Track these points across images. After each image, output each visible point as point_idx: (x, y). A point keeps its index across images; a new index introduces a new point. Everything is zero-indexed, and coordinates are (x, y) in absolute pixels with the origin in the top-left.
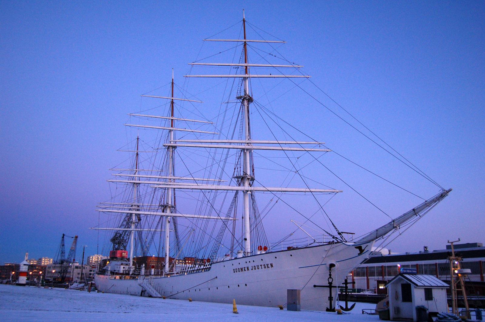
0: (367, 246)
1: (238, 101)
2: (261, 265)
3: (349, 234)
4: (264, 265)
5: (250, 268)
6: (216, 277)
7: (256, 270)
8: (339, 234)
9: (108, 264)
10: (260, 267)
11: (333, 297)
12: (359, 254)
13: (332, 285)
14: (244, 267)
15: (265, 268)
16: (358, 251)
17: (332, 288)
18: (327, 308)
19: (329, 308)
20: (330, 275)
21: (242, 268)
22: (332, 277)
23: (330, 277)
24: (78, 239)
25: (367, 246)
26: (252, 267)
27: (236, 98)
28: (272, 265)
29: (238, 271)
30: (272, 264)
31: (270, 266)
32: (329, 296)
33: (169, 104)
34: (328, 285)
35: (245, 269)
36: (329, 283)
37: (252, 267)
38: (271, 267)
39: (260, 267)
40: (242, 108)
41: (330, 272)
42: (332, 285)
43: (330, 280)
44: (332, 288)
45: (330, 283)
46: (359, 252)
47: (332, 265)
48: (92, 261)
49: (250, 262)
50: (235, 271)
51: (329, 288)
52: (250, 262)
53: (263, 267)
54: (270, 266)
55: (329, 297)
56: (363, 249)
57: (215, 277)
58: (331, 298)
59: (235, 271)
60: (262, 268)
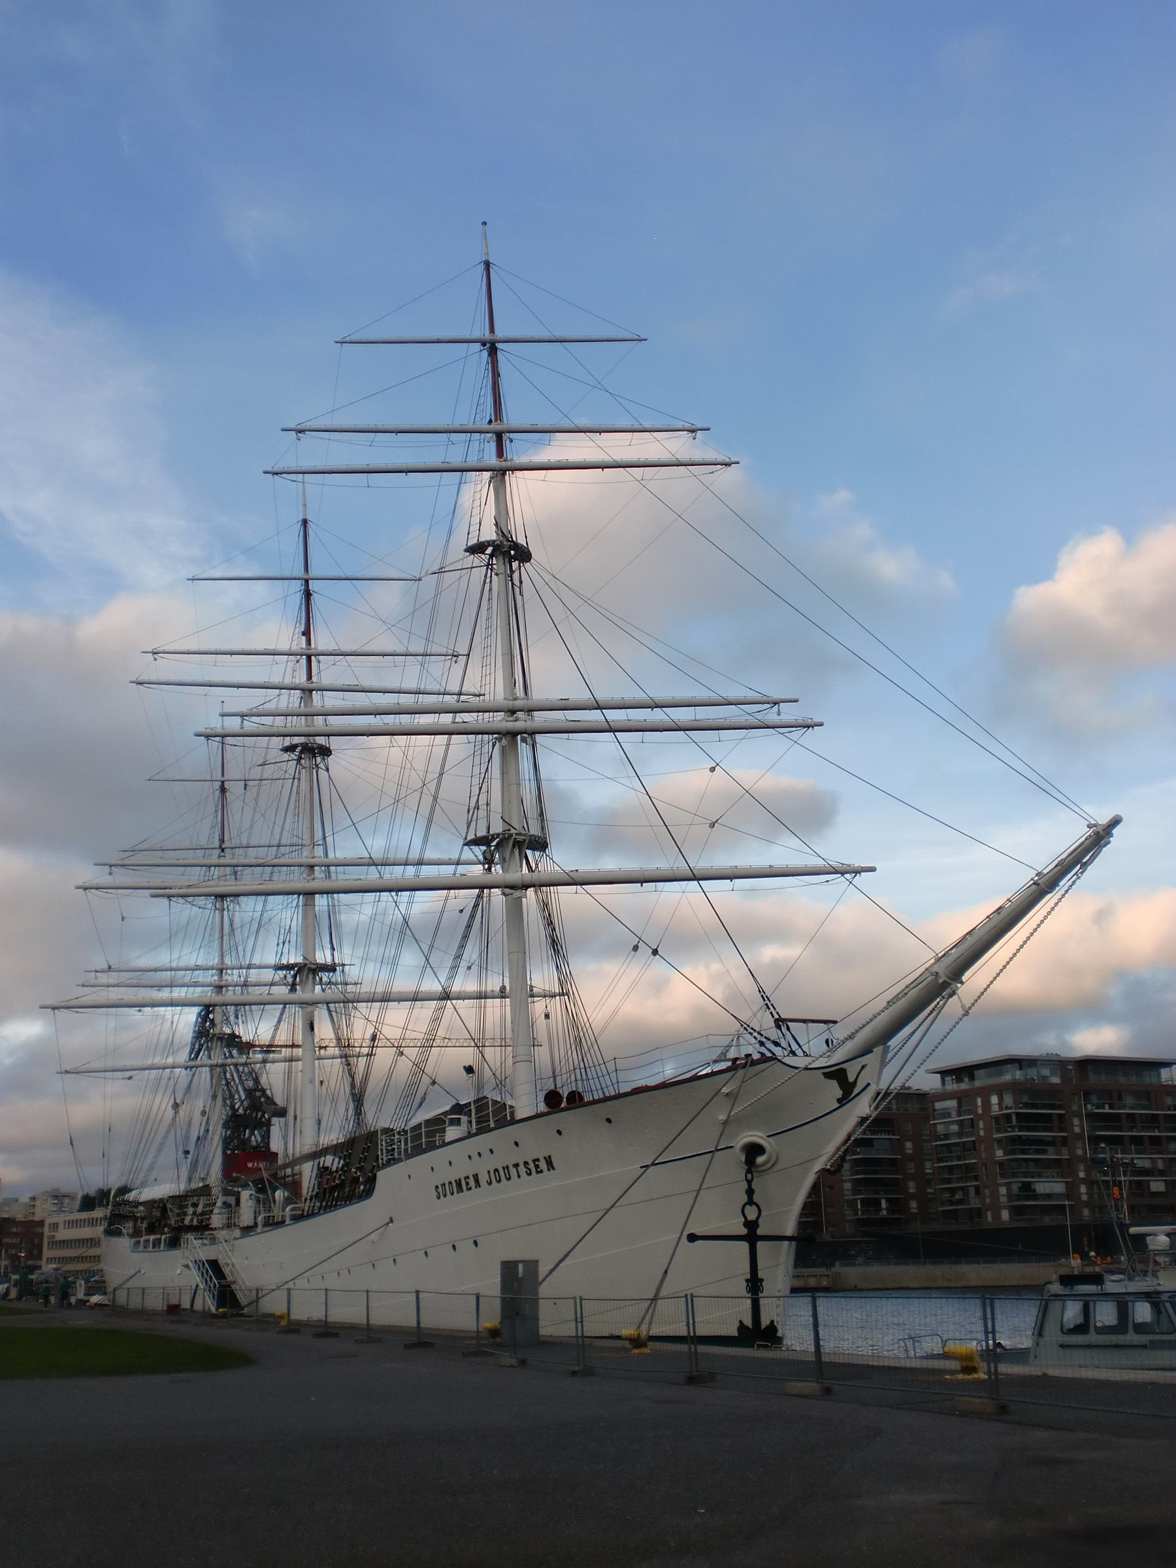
0: (863, 1067)
1: (286, 756)
2: (516, 1166)
3: (810, 1025)
4: (526, 1163)
5: (483, 1179)
6: (391, 1221)
7: (532, 1176)
8: (779, 1022)
9: (856, 1150)
10: (513, 1171)
11: (762, 1280)
12: (839, 1100)
13: (760, 1232)
14: (466, 1175)
15: (476, 1177)
16: (834, 1090)
17: (759, 1244)
18: (741, 1321)
19: (748, 1322)
20: (750, 1192)
21: (460, 1179)
22: (756, 1198)
23: (751, 1202)
24: (310, 524)
25: (863, 1067)
26: (489, 1172)
27: (466, 551)
28: (550, 1164)
29: (448, 1193)
30: (550, 1157)
31: (543, 1165)
32: (748, 1276)
33: (298, 527)
34: (744, 1231)
35: (537, 1167)
36: (747, 1224)
37: (489, 1172)
38: (549, 1170)
39: (513, 1171)
40: (487, 586)
41: (749, 1182)
42: (760, 1232)
43: (751, 1214)
44: (759, 1244)
45: (751, 1225)
46: (839, 1093)
47: (753, 1150)
48: (257, 1141)
49: (479, 1154)
50: (442, 1191)
51: (744, 1246)
52: (479, 1154)
53: (522, 1169)
54: (543, 1165)
55: (747, 1281)
56: (851, 1079)
57: (388, 1220)
58: (755, 1284)
59: (442, 1191)
60: (519, 1176)
